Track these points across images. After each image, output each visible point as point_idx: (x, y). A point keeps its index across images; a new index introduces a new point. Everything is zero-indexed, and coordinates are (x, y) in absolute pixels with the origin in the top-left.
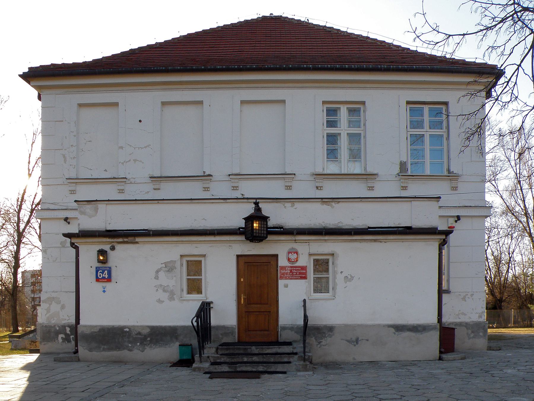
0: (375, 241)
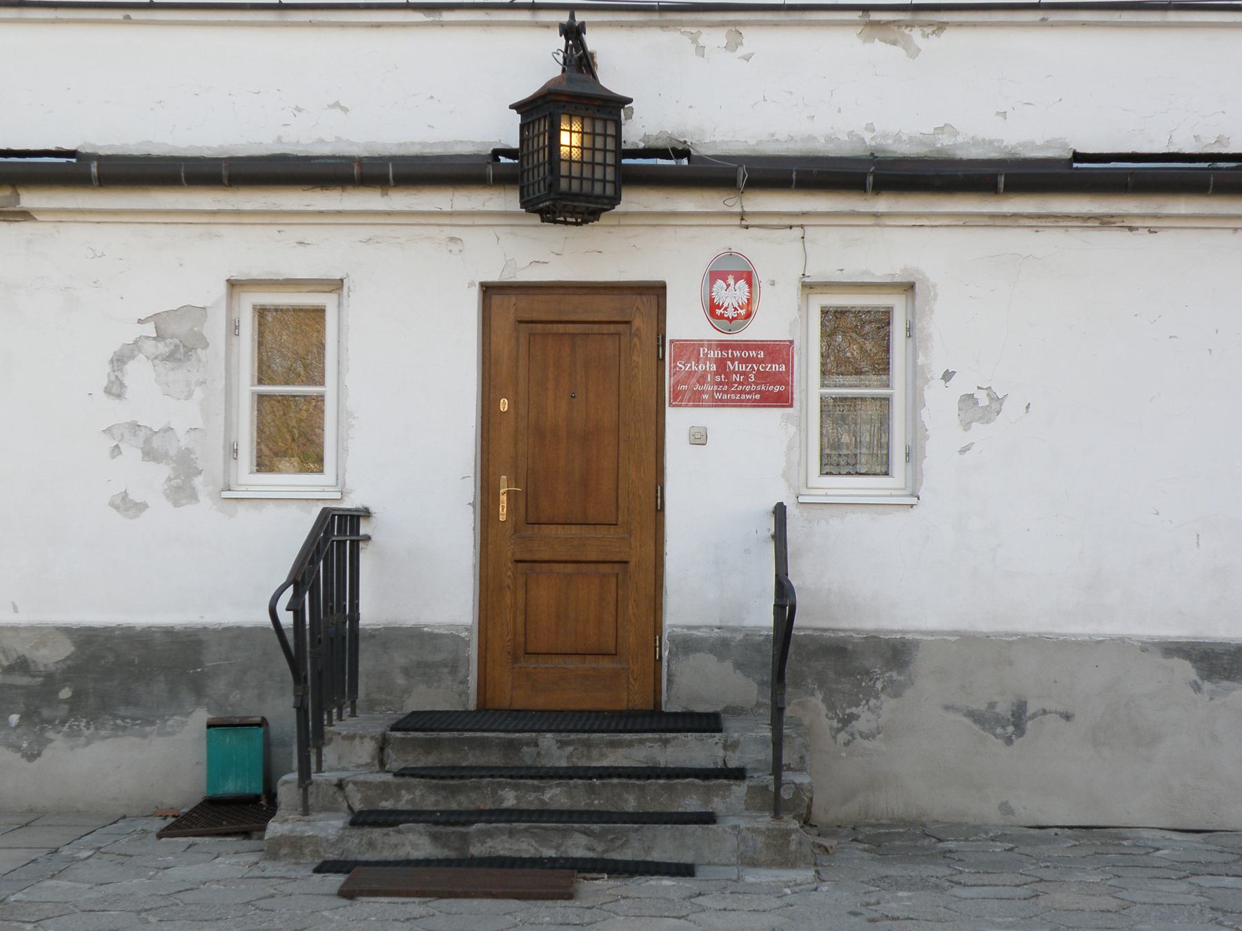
0: (1105, 221)
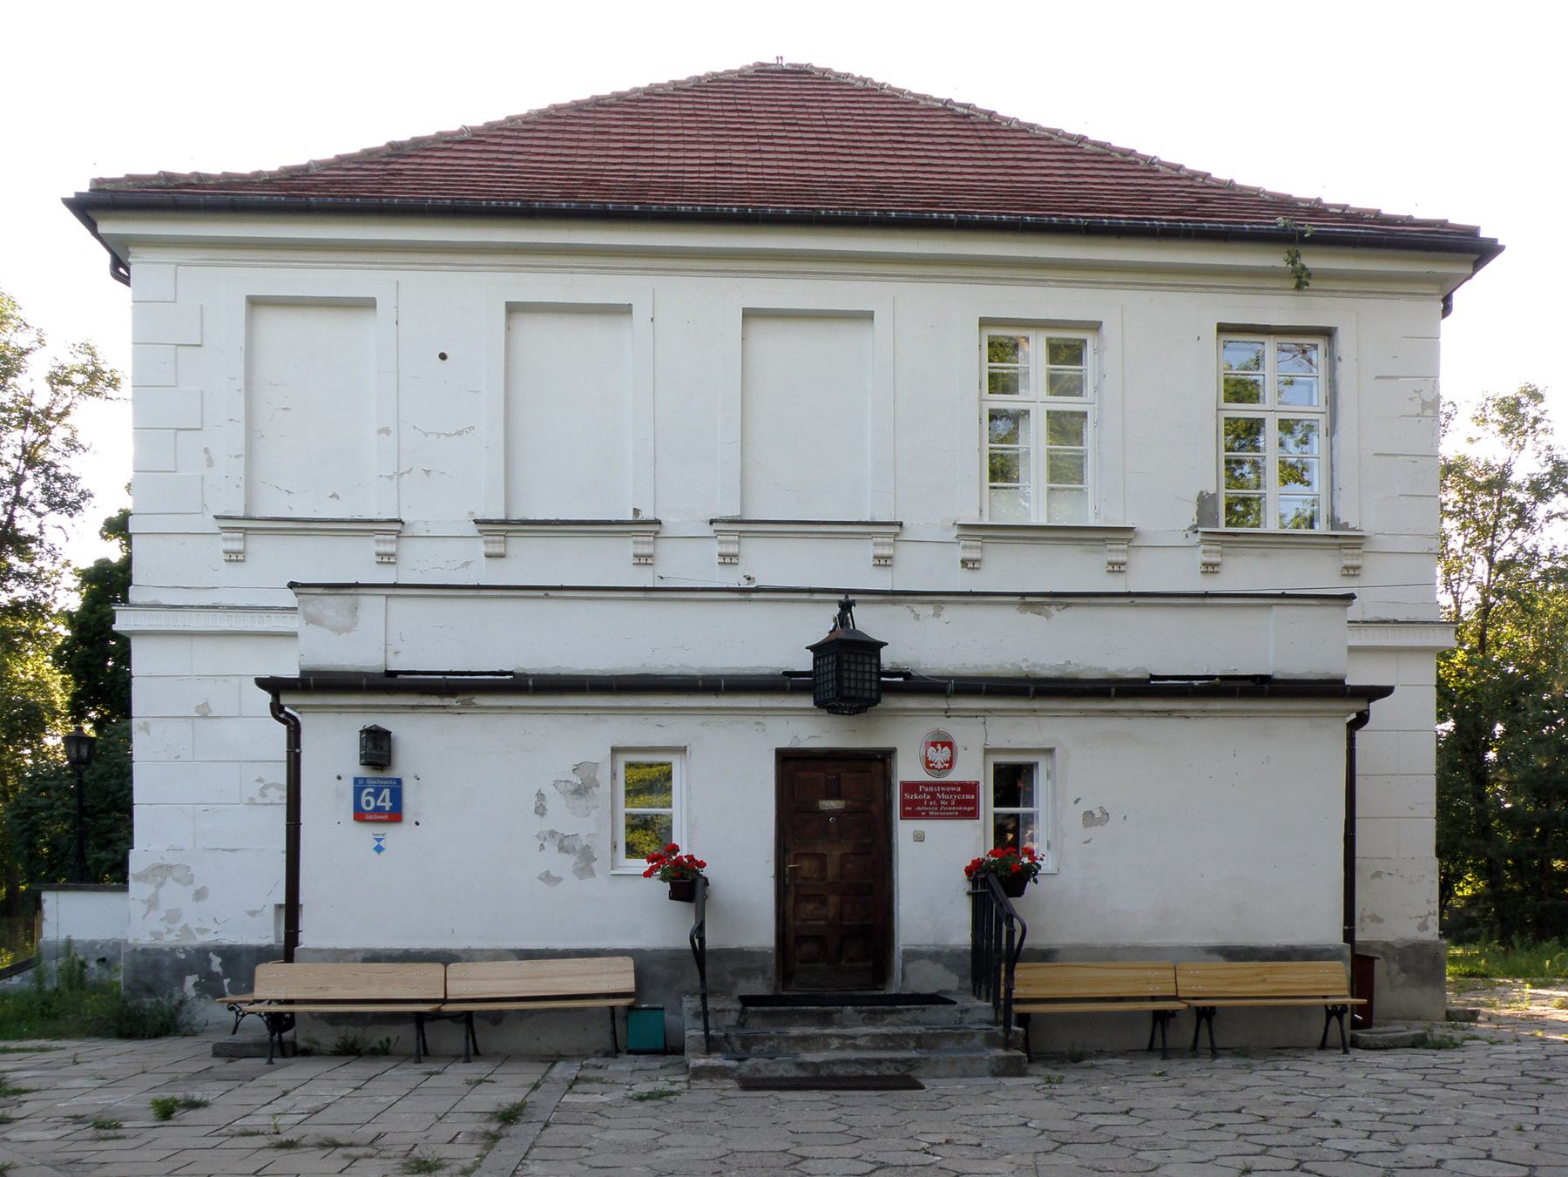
0: (1169, 713)
